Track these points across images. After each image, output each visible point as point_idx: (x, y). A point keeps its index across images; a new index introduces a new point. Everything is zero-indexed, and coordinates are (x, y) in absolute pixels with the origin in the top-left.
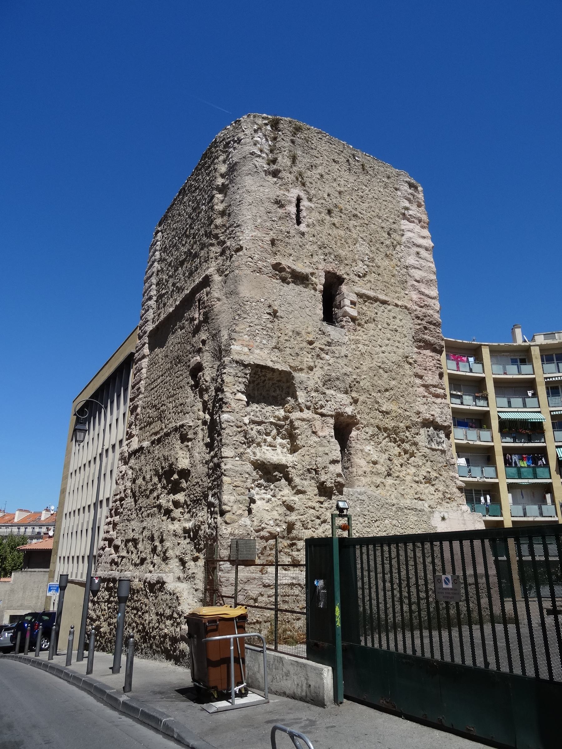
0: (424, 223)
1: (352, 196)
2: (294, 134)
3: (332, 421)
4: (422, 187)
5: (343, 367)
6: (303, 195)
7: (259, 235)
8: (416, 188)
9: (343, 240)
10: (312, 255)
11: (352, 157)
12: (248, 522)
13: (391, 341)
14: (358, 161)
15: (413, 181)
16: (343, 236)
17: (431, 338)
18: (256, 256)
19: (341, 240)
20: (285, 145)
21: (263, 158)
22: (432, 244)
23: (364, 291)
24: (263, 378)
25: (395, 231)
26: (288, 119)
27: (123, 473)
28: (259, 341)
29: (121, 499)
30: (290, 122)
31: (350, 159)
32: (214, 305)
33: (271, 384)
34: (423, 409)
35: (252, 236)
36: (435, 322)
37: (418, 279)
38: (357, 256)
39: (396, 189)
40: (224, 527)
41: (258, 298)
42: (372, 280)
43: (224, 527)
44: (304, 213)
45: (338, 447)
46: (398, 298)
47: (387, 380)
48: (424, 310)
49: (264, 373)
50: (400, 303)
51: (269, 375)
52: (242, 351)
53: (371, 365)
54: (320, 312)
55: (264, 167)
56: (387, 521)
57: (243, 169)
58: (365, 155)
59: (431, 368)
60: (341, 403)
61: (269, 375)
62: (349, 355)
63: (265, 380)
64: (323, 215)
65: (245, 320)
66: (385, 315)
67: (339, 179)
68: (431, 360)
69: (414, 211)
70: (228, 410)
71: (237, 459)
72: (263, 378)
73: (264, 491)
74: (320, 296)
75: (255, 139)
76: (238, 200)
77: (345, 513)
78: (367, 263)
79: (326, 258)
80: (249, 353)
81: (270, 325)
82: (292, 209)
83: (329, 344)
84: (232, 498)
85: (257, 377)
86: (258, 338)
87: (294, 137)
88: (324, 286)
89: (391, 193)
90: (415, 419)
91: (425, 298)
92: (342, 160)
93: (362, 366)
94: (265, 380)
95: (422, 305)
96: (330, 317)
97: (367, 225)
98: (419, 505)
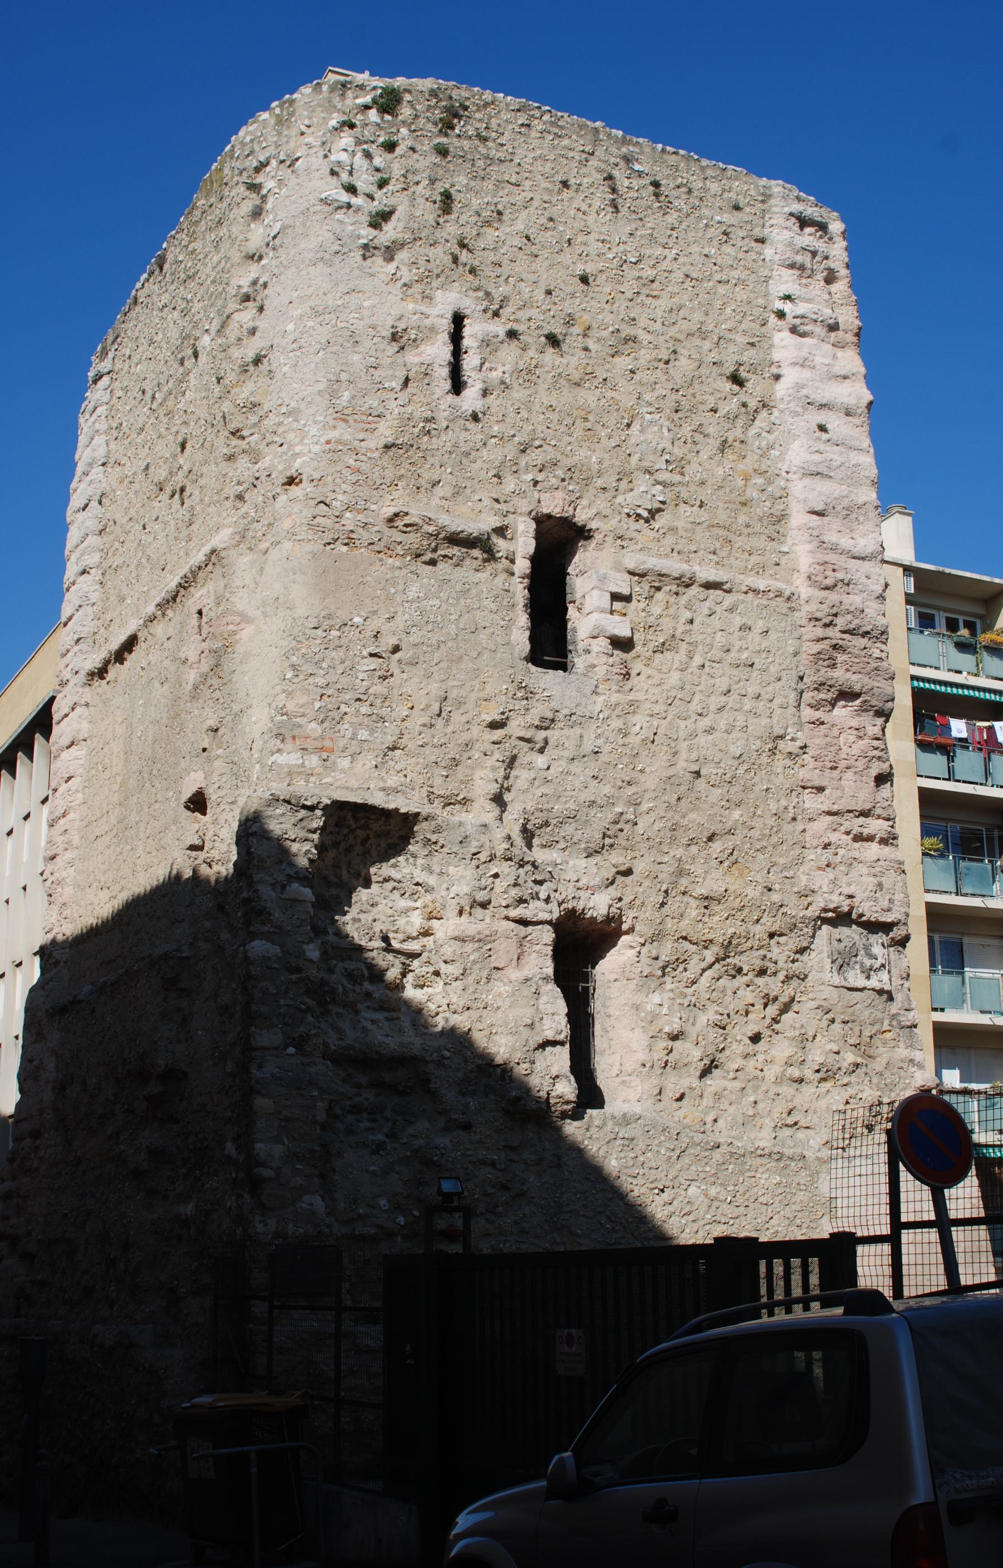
0: (846, 332)
1: (619, 283)
2: (447, 126)
3: (548, 935)
4: (843, 220)
5: (578, 786)
6: (469, 304)
7: (347, 437)
8: (822, 227)
9: (591, 417)
10: (498, 476)
11: (622, 163)
12: (319, 1204)
13: (733, 697)
14: (640, 174)
15: (812, 211)
16: (593, 406)
17: (855, 678)
18: (340, 497)
19: (586, 420)
20: (417, 166)
21: (358, 209)
22: (868, 397)
23: (652, 563)
24: (361, 834)
25: (753, 369)
26: (428, 83)
27: (35, 1063)
28: (349, 734)
29: (36, 1135)
30: (434, 93)
31: (616, 173)
32: (234, 633)
33: (383, 845)
34: (822, 881)
35: (328, 442)
36: (868, 628)
37: (819, 507)
38: (634, 460)
39: (762, 241)
40: (258, 1218)
41: (342, 615)
42: (680, 524)
43: (258, 1218)
44: (470, 362)
45: (562, 1007)
46: (760, 569)
47: (716, 809)
48: (833, 597)
49: (362, 822)
50: (761, 584)
51: (376, 826)
52: (303, 765)
53: (671, 772)
54: (521, 638)
55: (359, 237)
56: (693, 1190)
57: (302, 246)
58: (663, 151)
59: (852, 762)
60: (580, 884)
61: (376, 826)
62: (606, 749)
63: (368, 838)
64: (531, 353)
65: (311, 680)
66: (716, 622)
67: (580, 239)
68: (852, 738)
69: (814, 300)
70: (265, 928)
71: (291, 1050)
72: (361, 834)
73: (366, 1124)
74: (520, 593)
75: (333, 158)
76: (291, 338)
77: (455, 1204)
78: (662, 476)
79: (540, 477)
80: (321, 770)
81: (379, 688)
82: (440, 350)
83: (546, 724)
84: (278, 1150)
85: (345, 831)
86: (346, 726)
87: (446, 135)
88: (534, 560)
89: (741, 255)
90: (795, 909)
91: (841, 561)
92: (591, 175)
93: (643, 778)
94: (368, 838)
95: (829, 582)
96: (550, 642)
97: (667, 362)
98: (790, 1142)
